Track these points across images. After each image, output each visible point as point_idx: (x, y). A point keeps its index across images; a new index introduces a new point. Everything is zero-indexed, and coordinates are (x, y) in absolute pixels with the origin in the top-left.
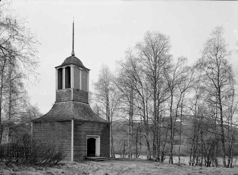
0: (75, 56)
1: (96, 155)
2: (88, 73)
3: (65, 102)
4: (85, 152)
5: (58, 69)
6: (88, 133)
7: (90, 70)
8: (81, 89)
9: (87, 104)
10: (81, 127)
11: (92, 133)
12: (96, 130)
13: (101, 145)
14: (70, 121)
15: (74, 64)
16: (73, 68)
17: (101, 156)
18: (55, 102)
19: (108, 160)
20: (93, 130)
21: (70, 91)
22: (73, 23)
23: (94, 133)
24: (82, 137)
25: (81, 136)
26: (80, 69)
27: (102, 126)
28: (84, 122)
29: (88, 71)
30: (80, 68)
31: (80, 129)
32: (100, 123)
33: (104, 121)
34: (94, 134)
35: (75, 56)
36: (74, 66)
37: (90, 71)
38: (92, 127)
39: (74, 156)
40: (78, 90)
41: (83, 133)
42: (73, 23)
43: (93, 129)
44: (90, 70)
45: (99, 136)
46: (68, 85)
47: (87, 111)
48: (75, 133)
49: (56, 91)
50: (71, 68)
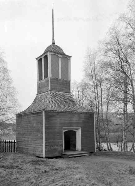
0: (55, 44)
1: (77, 149)
2: (69, 60)
3: (43, 94)
4: (61, 147)
5: (38, 60)
6: (64, 125)
7: (71, 57)
8: (60, 77)
9: (68, 94)
10: (54, 118)
11: (70, 125)
12: (75, 121)
13: (82, 138)
14: (41, 113)
15: (51, 51)
16: (50, 56)
17: (82, 150)
18: (37, 94)
19: (88, 156)
20: (71, 121)
21: (48, 81)
22: (53, 10)
23: (73, 125)
24: (57, 130)
25: (55, 128)
26: (59, 57)
27: (83, 117)
28: (58, 113)
29: (69, 58)
30: (59, 55)
31: (54, 121)
32: (80, 113)
33: (85, 111)
34: (72, 126)
35: (55, 44)
36: (51, 53)
37: (71, 58)
38: (70, 118)
39: (45, 151)
40: (57, 79)
41: (58, 125)
42: (53, 10)
43: (71, 120)
44: (71, 57)
45: (79, 129)
46: (46, 76)
47: (70, 101)
48: (47, 126)
49: (38, 82)
50: (48, 56)
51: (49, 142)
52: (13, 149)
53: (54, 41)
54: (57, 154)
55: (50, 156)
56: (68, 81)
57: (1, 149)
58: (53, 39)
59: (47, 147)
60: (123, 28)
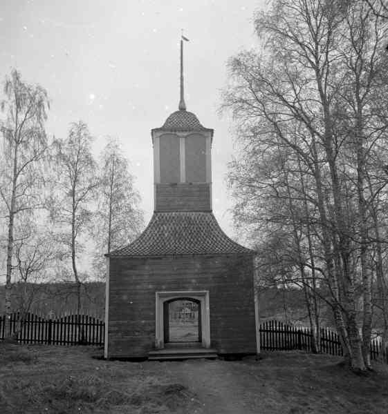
8: (183, 179)
43: (180, 274)
51: (118, 325)
52: (69, 329)
53: (184, 104)
54: (138, 351)
55: (120, 354)
56: (206, 184)
57: (2, 327)
58: (182, 100)
59: (113, 334)
60: (254, 45)
